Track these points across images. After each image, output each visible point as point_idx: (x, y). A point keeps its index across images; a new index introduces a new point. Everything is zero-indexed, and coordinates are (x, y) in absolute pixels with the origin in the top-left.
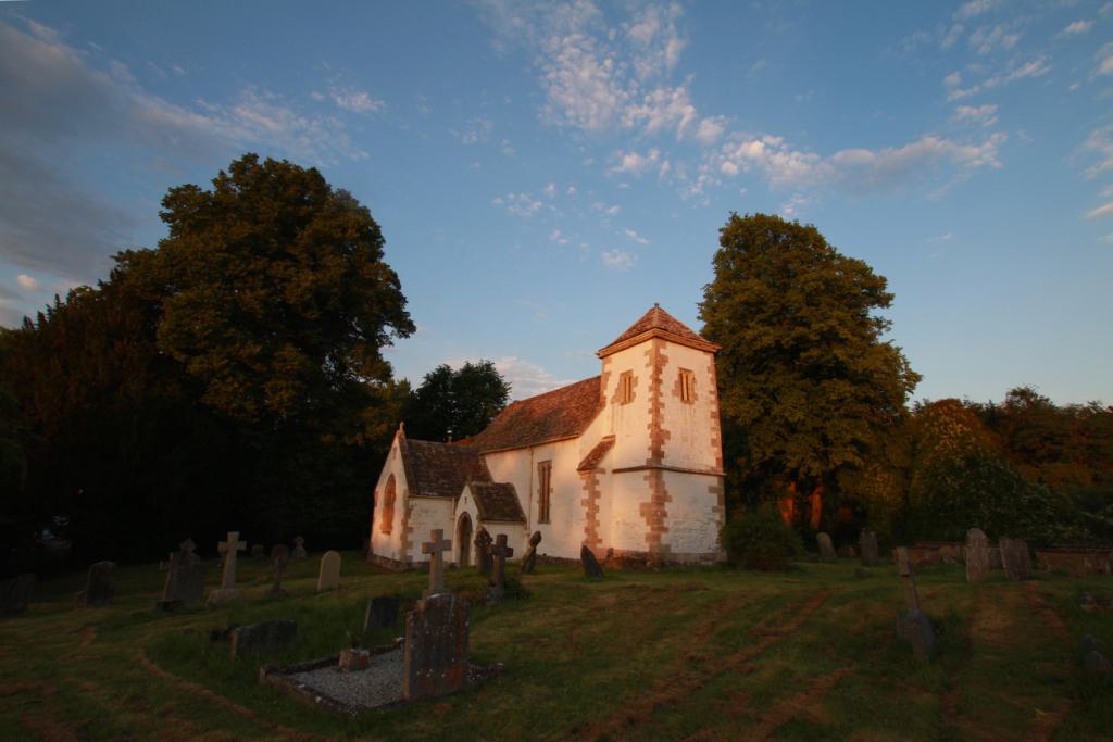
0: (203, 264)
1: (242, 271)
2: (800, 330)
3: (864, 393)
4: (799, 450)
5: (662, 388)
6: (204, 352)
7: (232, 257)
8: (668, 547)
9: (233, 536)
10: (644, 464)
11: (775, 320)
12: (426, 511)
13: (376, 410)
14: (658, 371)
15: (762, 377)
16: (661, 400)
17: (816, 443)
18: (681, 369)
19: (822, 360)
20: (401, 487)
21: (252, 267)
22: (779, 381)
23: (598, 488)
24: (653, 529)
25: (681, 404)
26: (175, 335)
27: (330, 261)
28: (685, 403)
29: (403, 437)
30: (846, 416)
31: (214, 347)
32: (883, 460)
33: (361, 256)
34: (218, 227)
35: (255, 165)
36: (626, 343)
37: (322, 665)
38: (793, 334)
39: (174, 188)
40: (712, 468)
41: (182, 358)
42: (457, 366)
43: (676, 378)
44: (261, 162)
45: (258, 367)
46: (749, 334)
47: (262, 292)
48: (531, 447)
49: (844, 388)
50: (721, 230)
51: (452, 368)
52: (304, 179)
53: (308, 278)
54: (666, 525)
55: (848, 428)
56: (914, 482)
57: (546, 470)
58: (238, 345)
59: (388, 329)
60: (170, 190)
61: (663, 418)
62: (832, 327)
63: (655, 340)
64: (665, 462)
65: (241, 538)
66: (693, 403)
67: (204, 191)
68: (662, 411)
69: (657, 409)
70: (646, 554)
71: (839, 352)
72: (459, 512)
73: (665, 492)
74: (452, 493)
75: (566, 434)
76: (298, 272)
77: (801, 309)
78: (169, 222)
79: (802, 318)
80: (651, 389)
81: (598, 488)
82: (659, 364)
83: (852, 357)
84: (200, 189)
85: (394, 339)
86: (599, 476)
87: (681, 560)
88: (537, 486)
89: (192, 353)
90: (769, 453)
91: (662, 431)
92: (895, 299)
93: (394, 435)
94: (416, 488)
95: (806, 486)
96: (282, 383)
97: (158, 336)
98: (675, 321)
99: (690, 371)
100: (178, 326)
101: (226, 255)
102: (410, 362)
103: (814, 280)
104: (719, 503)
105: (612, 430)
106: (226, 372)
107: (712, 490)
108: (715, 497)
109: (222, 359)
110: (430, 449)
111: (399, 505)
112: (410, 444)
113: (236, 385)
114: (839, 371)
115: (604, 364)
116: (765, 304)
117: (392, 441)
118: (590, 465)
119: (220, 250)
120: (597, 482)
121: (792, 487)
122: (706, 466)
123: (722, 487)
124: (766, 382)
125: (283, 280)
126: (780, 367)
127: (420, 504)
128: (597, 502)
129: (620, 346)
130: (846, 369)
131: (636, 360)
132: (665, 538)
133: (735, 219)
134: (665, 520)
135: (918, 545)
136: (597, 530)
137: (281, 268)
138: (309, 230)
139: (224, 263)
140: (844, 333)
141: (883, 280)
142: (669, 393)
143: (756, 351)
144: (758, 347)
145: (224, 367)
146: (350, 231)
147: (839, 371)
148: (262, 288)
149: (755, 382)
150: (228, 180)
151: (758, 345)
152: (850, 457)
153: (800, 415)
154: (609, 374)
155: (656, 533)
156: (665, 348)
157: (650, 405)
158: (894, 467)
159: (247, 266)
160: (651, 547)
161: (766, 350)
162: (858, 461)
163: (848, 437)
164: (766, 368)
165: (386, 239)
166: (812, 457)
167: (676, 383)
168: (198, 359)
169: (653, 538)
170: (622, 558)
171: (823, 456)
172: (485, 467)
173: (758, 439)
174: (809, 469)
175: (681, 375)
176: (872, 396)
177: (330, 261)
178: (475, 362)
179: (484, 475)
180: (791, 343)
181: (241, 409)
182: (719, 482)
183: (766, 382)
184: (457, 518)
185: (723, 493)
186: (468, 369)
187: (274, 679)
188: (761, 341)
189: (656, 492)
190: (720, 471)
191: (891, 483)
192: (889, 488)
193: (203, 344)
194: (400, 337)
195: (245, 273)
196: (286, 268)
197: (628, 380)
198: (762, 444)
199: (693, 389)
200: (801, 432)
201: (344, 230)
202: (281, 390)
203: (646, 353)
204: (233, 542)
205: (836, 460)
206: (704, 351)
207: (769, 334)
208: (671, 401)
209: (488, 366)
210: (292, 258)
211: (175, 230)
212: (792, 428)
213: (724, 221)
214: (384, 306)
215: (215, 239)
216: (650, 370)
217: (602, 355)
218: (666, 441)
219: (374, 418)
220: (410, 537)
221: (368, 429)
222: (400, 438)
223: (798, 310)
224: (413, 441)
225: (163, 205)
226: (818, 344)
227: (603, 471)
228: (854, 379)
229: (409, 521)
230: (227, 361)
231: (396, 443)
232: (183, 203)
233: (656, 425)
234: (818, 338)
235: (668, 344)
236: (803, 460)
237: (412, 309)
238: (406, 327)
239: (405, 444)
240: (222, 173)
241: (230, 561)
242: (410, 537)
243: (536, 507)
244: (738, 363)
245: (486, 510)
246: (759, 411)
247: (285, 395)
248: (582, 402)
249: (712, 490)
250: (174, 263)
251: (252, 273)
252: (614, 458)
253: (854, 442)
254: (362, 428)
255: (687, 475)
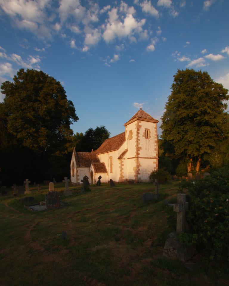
0: (15, 106)
1: (26, 107)
2: (196, 110)
3: (214, 130)
4: (192, 149)
5: (139, 135)
6: (20, 132)
7: (23, 103)
8: (140, 178)
9: (27, 180)
10: (134, 156)
11: (188, 107)
12: (82, 171)
13: (70, 144)
14: (138, 130)
15: (182, 127)
16: (139, 138)
17: (198, 147)
18: (146, 129)
19: (201, 120)
20: (75, 165)
21: (29, 105)
22: (187, 127)
23: (123, 163)
24: (136, 174)
25: (145, 139)
26: (12, 128)
27: (50, 101)
28: (147, 139)
29: (75, 151)
30: (208, 138)
31: (23, 130)
32: (218, 151)
33: (59, 98)
34: (17, 94)
35: (24, 72)
36: (131, 122)
37: (37, 205)
38: (193, 112)
39: (3, 83)
40: (154, 157)
41: (15, 134)
42: (94, 128)
43: (144, 131)
44: (25, 71)
45: (35, 135)
46: (178, 113)
47: (33, 113)
49: (208, 129)
50: (174, 76)
51: (93, 129)
52: (39, 75)
53: (44, 107)
54: (139, 172)
55: (207, 142)
56: (226, 157)
58: (29, 129)
59: (71, 120)
60: (2, 84)
61: (139, 144)
62: (205, 109)
63: (138, 121)
64: (139, 156)
65: (29, 180)
66: (149, 138)
67: (11, 83)
68: (139, 142)
69: (138, 141)
70: (134, 180)
71: (206, 118)
72: (90, 171)
73: (140, 164)
74: (88, 166)
75: (115, 149)
76: (42, 105)
77: (197, 103)
78: (4, 94)
79: (197, 106)
80: (136, 135)
81: (123, 163)
82: (139, 128)
83: (211, 118)
84: (10, 82)
85: (73, 122)
86: (123, 160)
87: (144, 181)
88: (110, 163)
89: (18, 132)
90: (182, 150)
91: (139, 147)
92: (160, 118)
93: (72, 152)
94: (79, 165)
95: (195, 159)
96: (43, 139)
97: (8, 128)
98: (146, 113)
99: (149, 129)
100: (12, 125)
101: (21, 103)
102: (79, 128)
103: (202, 93)
104: (156, 166)
105: (127, 147)
106: (27, 137)
107: (154, 163)
109: (25, 134)
110: (83, 154)
112: (77, 153)
113: (30, 140)
114: (207, 124)
116: (185, 102)
117: (72, 153)
118: (121, 157)
119: (19, 102)
120: (123, 162)
121: (191, 160)
122: (153, 156)
123: (157, 162)
124: (184, 128)
125: (38, 108)
126: (189, 123)
127: (80, 169)
128: (123, 167)
129: (129, 123)
130: (209, 122)
131: (132, 127)
132: (139, 176)
133: (179, 71)
134: (139, 171)
136: (123, 174)
137: (37, 105)
138: (42, 92)
139: (21, 105)
140: (209, 111)
141: (227, 90)
142: (142, 136)
143: (181, 118)
144: (181, 117)
145: (26, 135)
146: (54, 91)
147: (207, 124)
148: (32, 111)
149: (181, 128)
150: (17, 78)
151: (181, 117)
152: (206, 151)
153: (192, 138)
154: (127, 131)
155: (136, 175)
156: (141, 123)
157: (136, 140)
158: (221, 153)
159: (27, 105)
160: (136, 178)
161: (184, 118)
162: (209, 151)
163: (206, 145)
164: (184, 124)
165: (66, 92)
166: (195, 151)
167: (144, 133)
168: (19, 134)
169: (136, 176)
171: (198, 150)
173: (180, 146)
174: (194, 155)
175: (146, 131)
176: (217, 131)
177: (50, 101)
178: (99, 127)
180: (192, 115)
181: (33, 147)
182: (157, 161)
183: (184, 128)
184: (90, 172)
185: (157, 163)
186: (98, 129)
187: (26, 207)
188: (182, 115)
189: (137, 164)
190: (157, 157)
191: (220, 158)
192: (219, 159)
193: (20, 129)
194: (75, 121)
195: (27, 108)
196: (38, 104)
197: (131, 132)
198: (180, 147)
199: (149, 134)
200: (193, 143)
201: (53, 91)
202: (42, 140)
203: (135, 125)
204: (27, 181)
205: (202, 152)
206: (154, 122)
207: (185, 113)
208: (142, 139)
209: (103, 127)
210: (39, 101)
211: (7, 95)
212: (190, 142)
213: (175, 73)
214: (69, 113)
215: (17, 98)
216: (136, 130)
217: (125, 125)
218: (140, 150)
219: (70, 146)
220: (78, 177)
221: (68, 149)
222: (74, 152)
223: (196, 104)
224: (78, 152)
225: (1, 89)
226: (201, 115)
227: (125, 159)
228: (211, 126)
229: (78, 174)
230: (26, 134)
231: (73, 153)
232: (6, 87)
233: (137, 146)
234: (200, 113)
235: (142, 121)
236: (192, 152)
237: (77, 113)
238: (76, 119)
239: (76, 153)
240: (15, 76)
241: (27, 186)
242: (78, 177)
243: (110, 169)
244: (175, 123)
245: (96, 170)
246: (180, 137)
247: (44, 142)
248: (121, 139)
249: (154, 163)
250: (7, 107)
251: (29, 107)
252: (127, 156)
253: (209, 146)
254: (66, 149)
255: (150, 159)
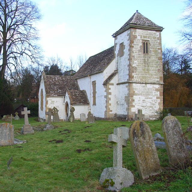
9: (25, 109)
48: (90, 75)
57: (94, 83)
88: (92, 91)
107: (157, 90)
108: (158, 93)
111: (44, 100)
115: (115, 40)
135: (6, 78)
170: (119, 117)
172: (77, 84)
179: (76, 87)
224: (47, 75)
227: (113, 84)
233: (130, 65)
235: (137, 30)
249: (157, 90)
